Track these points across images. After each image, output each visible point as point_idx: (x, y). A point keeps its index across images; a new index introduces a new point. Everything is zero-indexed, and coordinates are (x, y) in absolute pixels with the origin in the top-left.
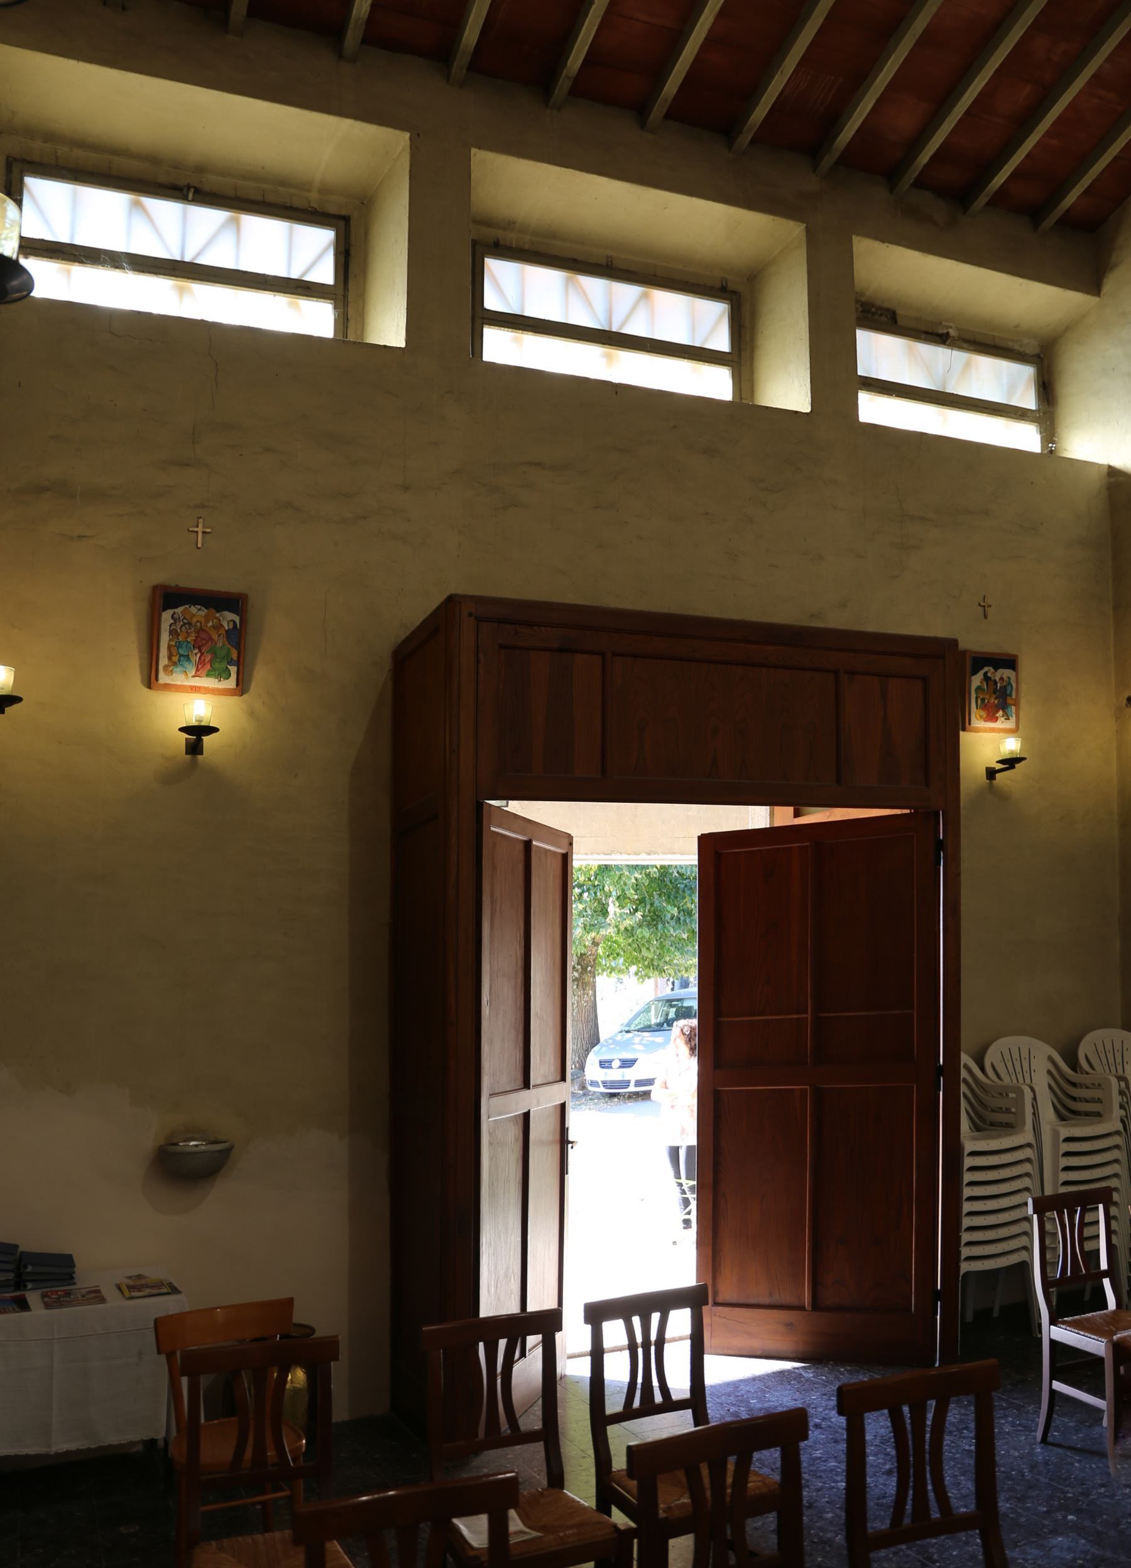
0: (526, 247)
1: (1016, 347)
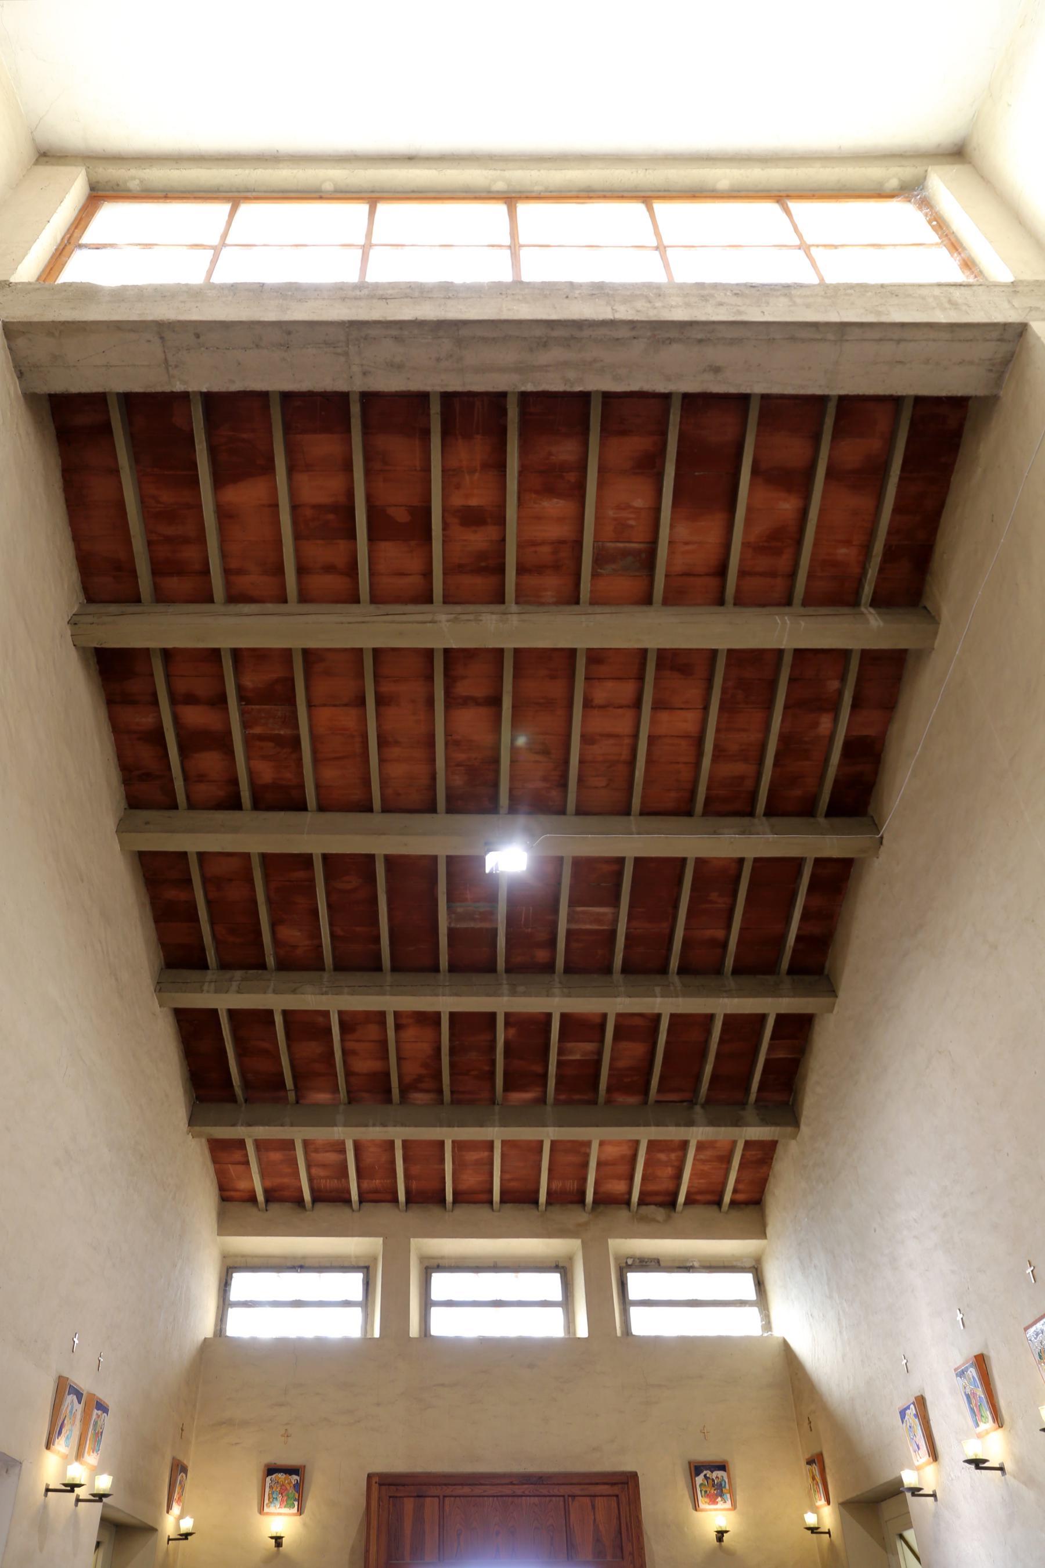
0: (453, 1265)
1: (739, 1264)
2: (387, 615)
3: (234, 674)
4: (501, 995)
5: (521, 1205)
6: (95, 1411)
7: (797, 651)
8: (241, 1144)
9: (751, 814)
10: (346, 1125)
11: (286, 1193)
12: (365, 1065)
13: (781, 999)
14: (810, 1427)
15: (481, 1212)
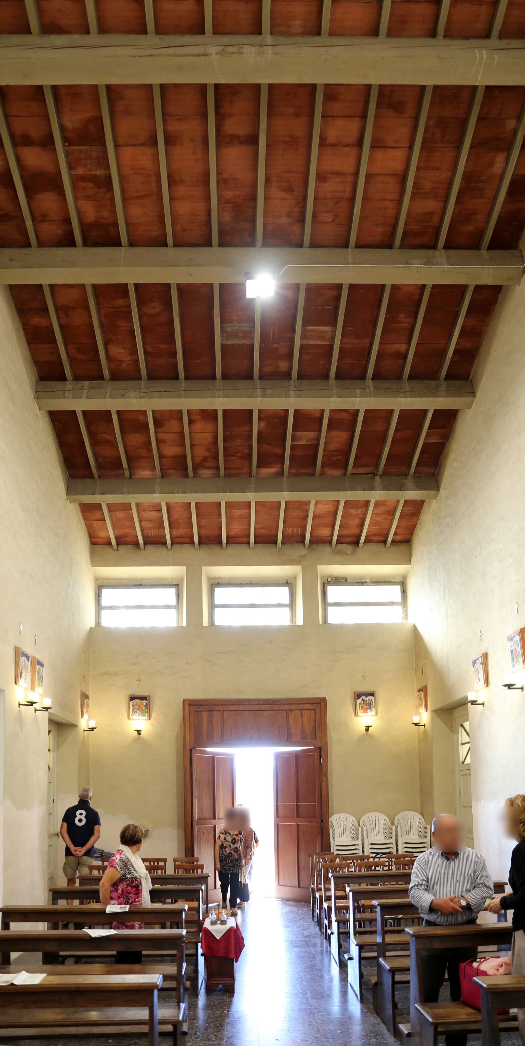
0: (227, 583)
1: (393, 580)
2: (170, 47)
3: (57, 119)
4: (256, 397)
5: (266, 545)
6: (37, 666)
7: (488, 87)
8: (98, 507)
9: (434, 247)
10: (161, 492)
11: (128, 539)
12: (171, 450)
13: (438, 398)
14: (422, 672)
15: (242, 550)
